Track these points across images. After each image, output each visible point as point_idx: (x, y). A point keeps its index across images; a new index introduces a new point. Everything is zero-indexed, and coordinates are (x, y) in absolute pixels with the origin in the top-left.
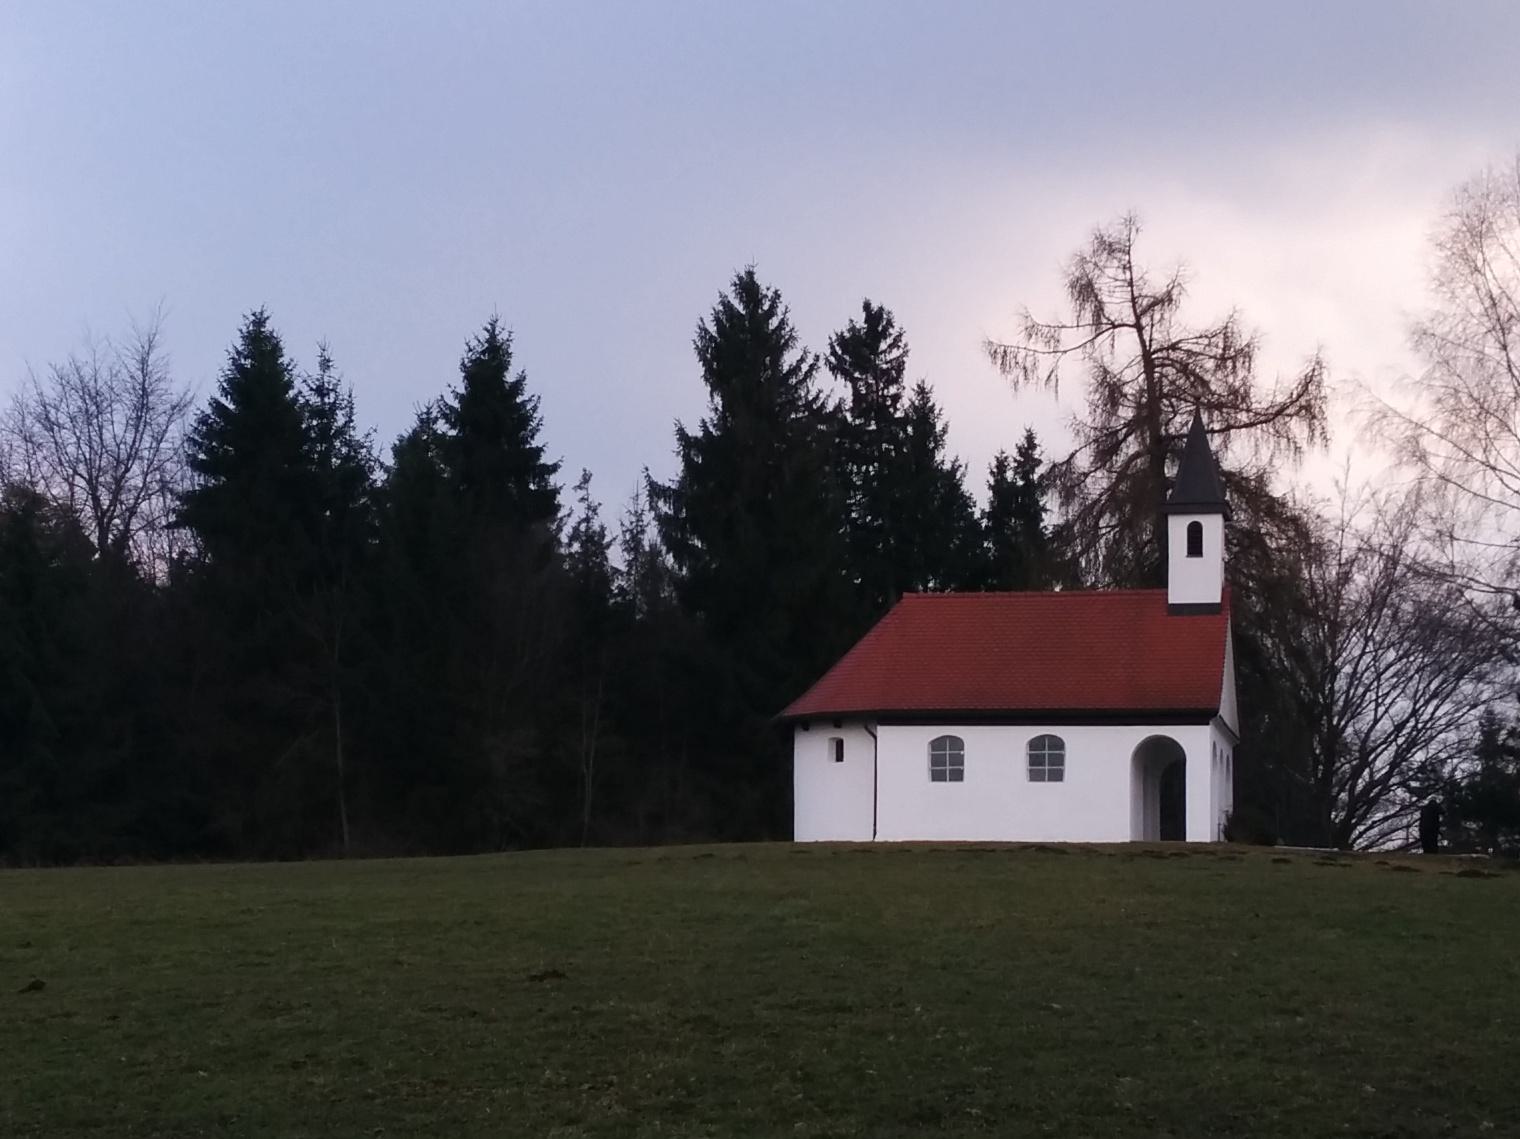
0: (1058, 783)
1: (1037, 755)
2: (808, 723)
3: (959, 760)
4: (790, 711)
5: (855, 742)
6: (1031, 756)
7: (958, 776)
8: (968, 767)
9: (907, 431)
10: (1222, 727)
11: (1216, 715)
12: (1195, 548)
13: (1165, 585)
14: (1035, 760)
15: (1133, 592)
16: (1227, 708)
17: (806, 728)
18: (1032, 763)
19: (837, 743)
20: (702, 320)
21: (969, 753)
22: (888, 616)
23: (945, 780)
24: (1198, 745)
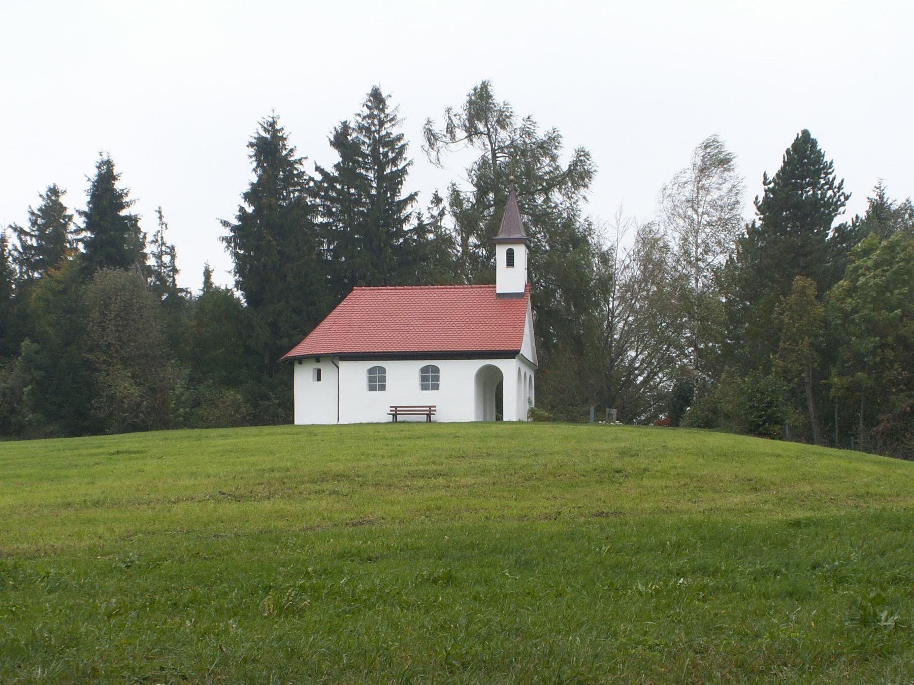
0: (383, 392)
1: (425, 376)
2: (301, 360)
3: (383, 379)
4: (295, 352)
5: (327, 371)
6: (422, 377)
7: (383, 388)
8: (442, 382)
9: (27, 276)
10: (524, 360)
11: (519, 353)
12: (510, 262)
13: (495, 283)
14: (424, 379)
15: (470, 286)
16: (527, 349)
17: (300, 363)
18: (422, 381)
19: (316, 371)
20: (30, 207)
21: (388, 375)
22: (345, 300)
23: (376, 390)
24: (509, 369)
